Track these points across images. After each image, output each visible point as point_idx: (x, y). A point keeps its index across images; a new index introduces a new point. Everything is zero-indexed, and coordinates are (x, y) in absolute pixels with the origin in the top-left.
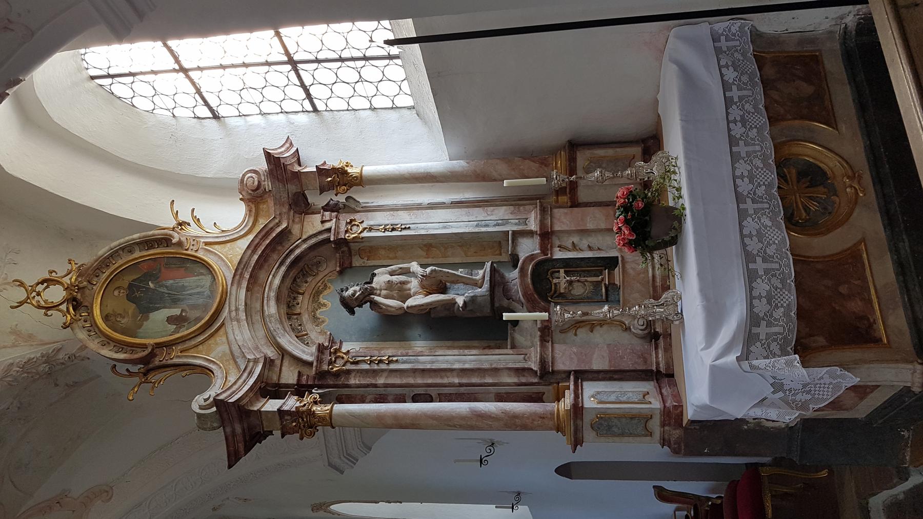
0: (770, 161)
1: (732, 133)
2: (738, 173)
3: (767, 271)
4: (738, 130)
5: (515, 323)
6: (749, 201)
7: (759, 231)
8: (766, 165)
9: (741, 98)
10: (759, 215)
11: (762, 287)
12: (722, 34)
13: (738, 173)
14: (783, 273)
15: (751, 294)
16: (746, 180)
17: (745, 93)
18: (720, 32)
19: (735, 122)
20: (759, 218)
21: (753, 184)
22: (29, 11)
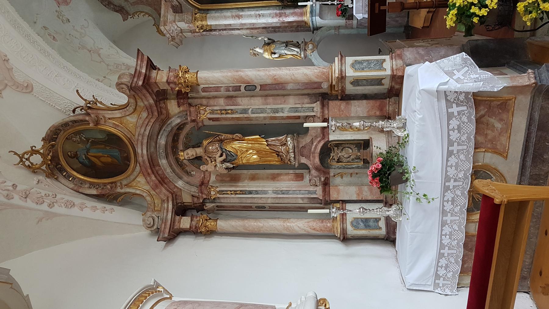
0: (459, 260)
1: (443, 242)
2: (440, 264)
3: (459, 113)
4: (442, 272)
5: (308, 128)
6: (449, 214)
7: (453, 199)
8: (457, 262)
9: (458, 151)
10: (445, 287)
11: (454, 123)
12: (442, 277)
13: (446, 199)
14: (460, 222)
15: (438, 265)
16: (448, 237)
17: (452, 251)
18: (454, 140)
19: (442, 267)
20: (461, 118)
21: (460, 133)
22: (35, 23)
